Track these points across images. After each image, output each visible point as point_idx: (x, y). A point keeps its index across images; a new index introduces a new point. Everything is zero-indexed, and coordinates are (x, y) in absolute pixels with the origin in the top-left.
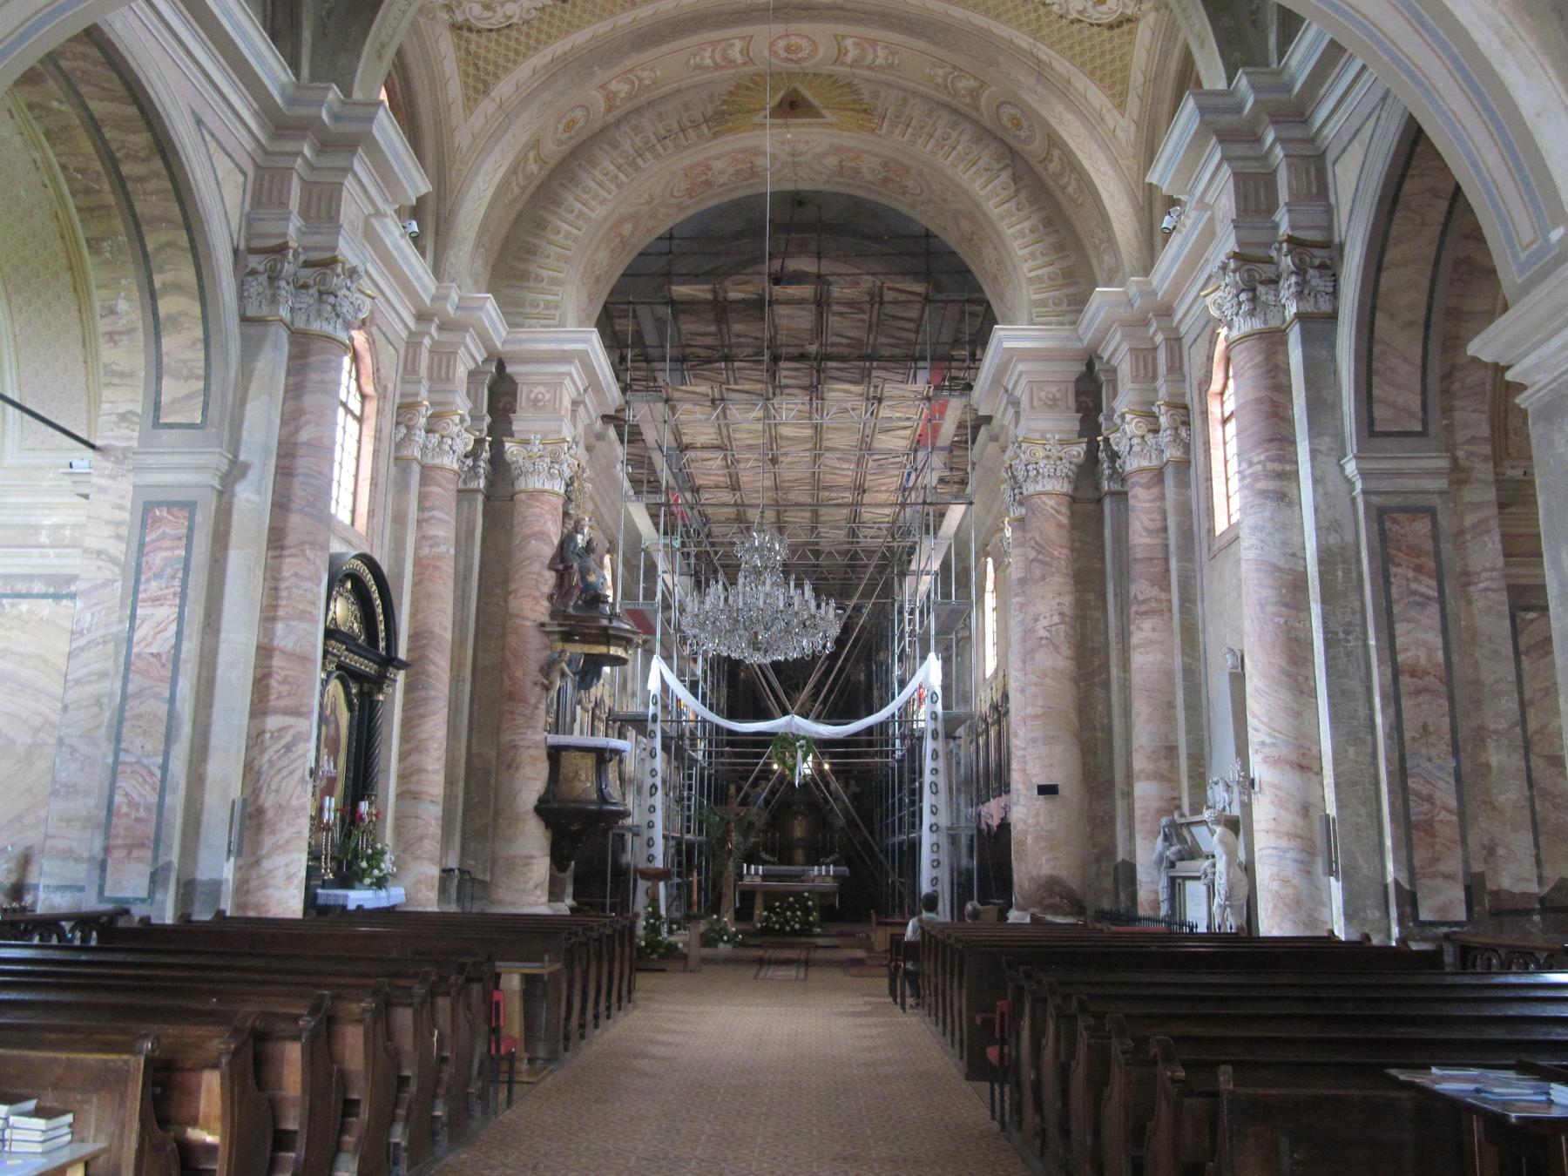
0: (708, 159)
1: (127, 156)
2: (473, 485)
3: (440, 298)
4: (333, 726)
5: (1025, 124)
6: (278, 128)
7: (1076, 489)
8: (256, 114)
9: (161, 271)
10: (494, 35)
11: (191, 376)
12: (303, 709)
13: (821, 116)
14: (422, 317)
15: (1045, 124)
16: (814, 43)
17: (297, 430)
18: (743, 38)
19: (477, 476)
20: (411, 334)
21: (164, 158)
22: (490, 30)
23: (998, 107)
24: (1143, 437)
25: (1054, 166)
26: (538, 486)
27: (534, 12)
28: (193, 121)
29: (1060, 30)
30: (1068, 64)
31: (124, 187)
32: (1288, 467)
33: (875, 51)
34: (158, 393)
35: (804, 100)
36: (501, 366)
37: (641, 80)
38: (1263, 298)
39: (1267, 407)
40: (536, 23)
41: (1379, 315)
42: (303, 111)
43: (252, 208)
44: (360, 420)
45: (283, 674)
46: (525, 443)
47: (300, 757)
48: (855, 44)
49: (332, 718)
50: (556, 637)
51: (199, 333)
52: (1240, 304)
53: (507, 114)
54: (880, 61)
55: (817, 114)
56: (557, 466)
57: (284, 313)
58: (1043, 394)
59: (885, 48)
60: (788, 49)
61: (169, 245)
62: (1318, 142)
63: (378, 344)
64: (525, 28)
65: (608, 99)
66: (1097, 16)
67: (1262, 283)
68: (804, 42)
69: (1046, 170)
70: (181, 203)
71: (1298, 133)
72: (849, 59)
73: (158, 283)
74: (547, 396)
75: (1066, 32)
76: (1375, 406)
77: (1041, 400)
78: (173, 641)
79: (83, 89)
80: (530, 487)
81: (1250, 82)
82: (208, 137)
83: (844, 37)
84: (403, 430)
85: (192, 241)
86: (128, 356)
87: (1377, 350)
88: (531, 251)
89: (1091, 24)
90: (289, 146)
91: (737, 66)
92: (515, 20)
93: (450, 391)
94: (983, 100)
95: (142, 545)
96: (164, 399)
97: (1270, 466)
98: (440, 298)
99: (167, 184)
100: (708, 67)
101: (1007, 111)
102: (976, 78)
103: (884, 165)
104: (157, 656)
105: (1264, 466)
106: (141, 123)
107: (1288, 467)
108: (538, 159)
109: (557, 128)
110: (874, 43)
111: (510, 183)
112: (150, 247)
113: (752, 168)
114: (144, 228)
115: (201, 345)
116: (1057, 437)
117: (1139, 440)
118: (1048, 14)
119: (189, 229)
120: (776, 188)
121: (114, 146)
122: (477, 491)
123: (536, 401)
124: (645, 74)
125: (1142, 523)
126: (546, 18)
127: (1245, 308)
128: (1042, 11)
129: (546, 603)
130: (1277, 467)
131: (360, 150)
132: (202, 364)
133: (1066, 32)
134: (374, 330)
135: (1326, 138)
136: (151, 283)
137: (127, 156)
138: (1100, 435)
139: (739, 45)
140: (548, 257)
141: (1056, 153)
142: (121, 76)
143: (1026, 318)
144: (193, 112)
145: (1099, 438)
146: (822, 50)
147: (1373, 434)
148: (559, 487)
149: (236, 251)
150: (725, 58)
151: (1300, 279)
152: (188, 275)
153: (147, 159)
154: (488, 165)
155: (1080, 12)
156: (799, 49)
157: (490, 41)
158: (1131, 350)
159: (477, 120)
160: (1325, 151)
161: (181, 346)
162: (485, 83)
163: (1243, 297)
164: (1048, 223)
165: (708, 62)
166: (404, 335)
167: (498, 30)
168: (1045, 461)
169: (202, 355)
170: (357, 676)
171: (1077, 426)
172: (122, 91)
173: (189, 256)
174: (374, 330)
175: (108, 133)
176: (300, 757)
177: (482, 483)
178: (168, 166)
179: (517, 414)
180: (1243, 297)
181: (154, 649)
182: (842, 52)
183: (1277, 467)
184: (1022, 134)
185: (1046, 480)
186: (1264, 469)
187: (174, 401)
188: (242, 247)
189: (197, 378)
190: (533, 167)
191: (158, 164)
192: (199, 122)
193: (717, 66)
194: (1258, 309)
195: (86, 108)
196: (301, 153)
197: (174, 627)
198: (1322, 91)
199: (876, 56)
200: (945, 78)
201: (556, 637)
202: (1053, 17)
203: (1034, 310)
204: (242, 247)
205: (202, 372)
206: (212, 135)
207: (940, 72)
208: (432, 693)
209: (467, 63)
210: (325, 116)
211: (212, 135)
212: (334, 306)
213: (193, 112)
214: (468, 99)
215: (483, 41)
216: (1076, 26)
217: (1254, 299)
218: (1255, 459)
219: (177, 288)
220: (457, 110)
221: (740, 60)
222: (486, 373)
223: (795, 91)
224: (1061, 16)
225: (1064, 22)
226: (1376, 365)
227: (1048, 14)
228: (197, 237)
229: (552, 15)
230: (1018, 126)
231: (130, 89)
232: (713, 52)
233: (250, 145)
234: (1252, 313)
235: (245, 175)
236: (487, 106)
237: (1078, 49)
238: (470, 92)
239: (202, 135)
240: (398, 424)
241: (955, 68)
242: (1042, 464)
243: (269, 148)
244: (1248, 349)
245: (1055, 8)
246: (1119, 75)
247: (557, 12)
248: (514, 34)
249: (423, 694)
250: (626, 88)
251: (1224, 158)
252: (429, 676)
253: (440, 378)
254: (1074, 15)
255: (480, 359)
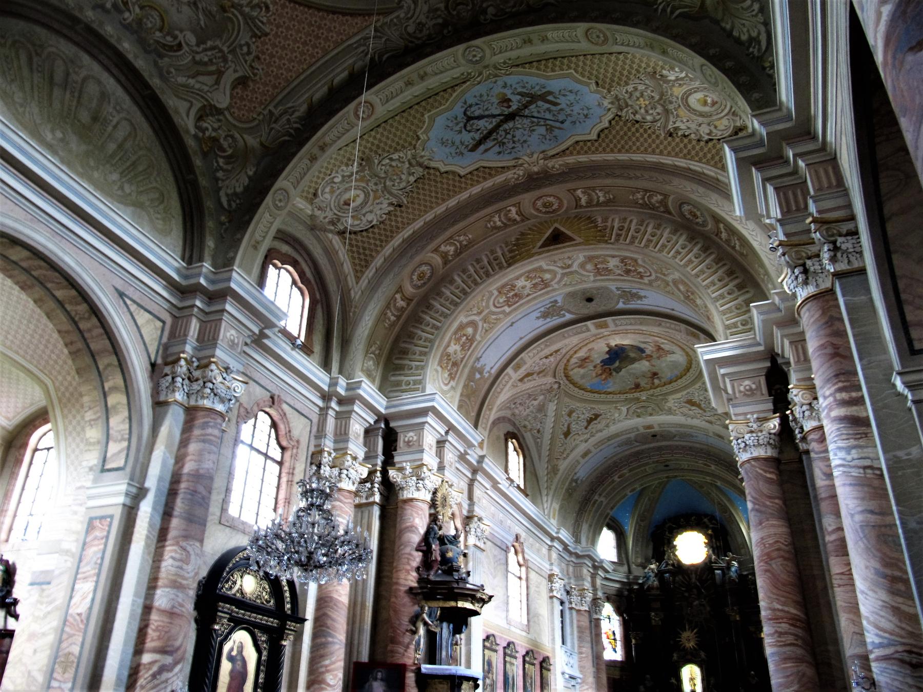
0: (511, 280)
1: (80, 318)
2: (371, 500)
3: (333, 383)
4: (239, 663)
5: (698, 213)
6: (210, 298)
7: (781, 452)
8: (165, 288)
9: (107, 381)
10: (364, 234)
11: (123, 439)
12: (168, 649)
13: (573, 240)
14: (326, 397)
15: (708, 210)
16: (558, 198)
17: (182, 467)
18: (514, 205)
19: (373, 494)
20: (321, 409)
21: (97, 316)
22: (362, 231)
23: (680, 209)
24: (810, 404)
25: (724, 235)
26: (410, 496)
27: (384, 216)
28: (116, 295)
29: (702, 149)
30: (713, 169)
31: (83, 336)
32: (854, 394)
33: (597, 194)
34: (106, 452)
35: (563, 233)
36: (387, 423)
37: (460, 243)
38: (812, 269)
39: (829, 350)
40: (387, 222)
41: (895, 257)
42: (193, 281)
43: (169, 339)
44: (280, 464)
45: (156, 624)
46: (401, 469)
47: (163, 682)
48: (583, 192)
49: (238, 658)
50: (421, 597)
51: (126, 414)
52: (797, 277)
53: (382, 273)
54: (602, 199)
55: (571, 239)
56: (421, 482)
57: (179, 396)
58: (742, 388)
59: (600, 190)
60: (544, 205)
61: (109, 365)
62: (828, 149)
63: (288, 416)
64: (382, 226)
65: (443, 257)
66: (720, 133)
67: (809, 258)
68: (551, 199)
69: (721, 239)
70: (109, 339)
71: (811, 146)
72: (583, 202)
73: (106, 388)
74: (415, 438)
75: (706, 149)
76: (910, 329)
77: (740, 392)
78: (88, 605)
79: (49, 285)
80: (405, 497)
81: (760, 122)
82: (129, 302)
83: (575, 190)
84: (314, 468)
85: (119, 360)
86: (94, 434)
87: (901, 285)
88: (404, 353)
89: (719, 140)
90: (188, 303)
91: (518, 223)
92: (374, 223)
93: (880, 526)
94: (670, 204)
95: (84, 544)
96: (109, 455)
97: (839, 396)
98: (333, 383)
99: (101, 331)
100: (500, 227)
101: (686, 208)
102: (661, 194)
103: (622, 261)
104: (80, 615)
105: (835, 397)
106: (80, 299)
107: (854, 394)
108: (404, 298)
109: (412, 279)
110: (593, 189)
111: (386, 314)
112: (101, 367)
113: (542, 281)
114: (97, 357)
115: (127, 421)
116: (755, 416)
117: (808, 407)
118: (690, 141)
119: (116, 354)
120: (284, 227)
121: (73, 314)
122: (374, 503)
123: (409, 442)
124: (462, 238)
125: (821, 469)
126: (393, 218)
127: (800, 280)
128: (686, 141)
129: (415, 574)
130: (844, 396)
131: (229, 298)
132: (127, 432)
133: (706, 149)
134: (285, 406)
135: (831, 143)
136: (103, 388)
137: (80, 318)
138: (788, 409)
139: (514, 210)
140: (415, 354)
141: (721, 226)
142: (60, 273)
143: (723, 337)
144: (116, 289)
145: (788, 412)
146: (565, 202)
147: (914, 352)
148: (428, 497)
149: (153, 365)
150: (509, 220)
151: (831, 246)
152: (119, 381)
153: (89, 318)
154: (371, 306)
155: (709, 134)
156: (551, 205)
157: (363, 237)
158: (791, 343)
159: (364, 282)
160: (835, 154)
161: (118, 423)
162: (366, 261)
163: (797, 271)
164: (730, 273)
165: (499, 223)
166: (317, 410)
167: (366, 230)
168: (749, 435)
169: (127, 426)
170: (264, 629)
171: (770, 406)
172: (65, 283)
173: (119, 369)
174: (285, 406)
175: (68, 307)
176: (163, 682)
177: (377, 498)
178: (99, 320)
179: (398, 451)
180: (797, 271)
181: (79, 611)
182: (578, 200)
183: (844, 396)
184: (700, 220)
185: (752, 449)
186: (835, 400)
187: (114, 455)
188: (159, 361)
189: (125, 440)
190: (401, 303)
191: (94, 320)
192: (121, 295)
193: (506, 226)
194: (810, 278)
195: (54, 296)
196: (194, 306)
197: (91, 596)
198: (812, 112)
199: (598, 197)
200: (643, 198)
201: (421, 597)
202: (694, 143)
203: (728, 331)
204: (159, 361)
205: (127, 436)
206: (134, 302)
207: (639, 196)
208: (330, 639)
209: (353, 252)
210: (202, 281)
211: (134, 302)
212: (212, 390)
213: (116, 289)
214: (357, 271)
215: (359, 238)
216: (710, 144)
217: (806, 271)
218: (828, 393)
219: (114, 389)
220: (351, 280)
221: (518, 218)
222: (378, 429)
223: (556, 229)
224: (699, 140)
225: (702, 143)
226: (903, 296)
227: (690, 141)
228: (121, 358)
229: (396, 216)
230: (695, 216)
231: (67, 280)
232: (499, 217)
233: (166, 305)
234: (806, 283)
235: (164, 322)
236: (370, 273)
237: (701, 154)
238: (358, 268)
239: (125, 303)
240: (311, 464)
241: (646, 191)
242: (747, 436)
243: (207, 309)
244: (808, 310)
245: (693, 136)
246: (717, 158)
247: (398, 213)
248: (376, 230)
249: (330, 639)
250: (452, 248)
251: (765, 180)
252: (328, 628)
253: (341, 434)
254: (707, 137)
255: (372, 422)
